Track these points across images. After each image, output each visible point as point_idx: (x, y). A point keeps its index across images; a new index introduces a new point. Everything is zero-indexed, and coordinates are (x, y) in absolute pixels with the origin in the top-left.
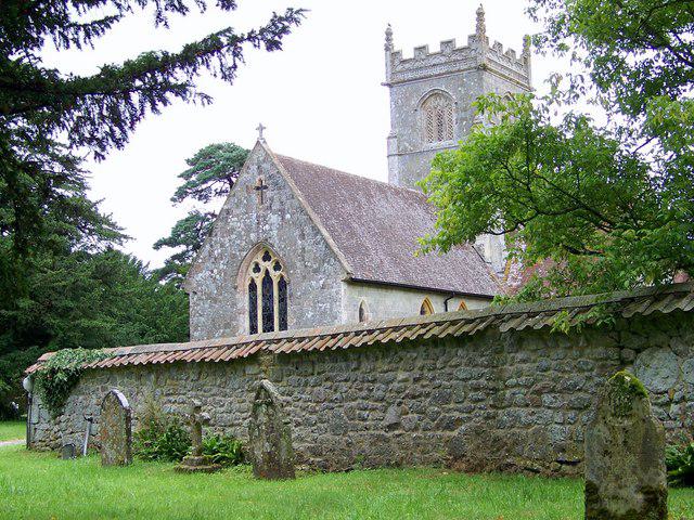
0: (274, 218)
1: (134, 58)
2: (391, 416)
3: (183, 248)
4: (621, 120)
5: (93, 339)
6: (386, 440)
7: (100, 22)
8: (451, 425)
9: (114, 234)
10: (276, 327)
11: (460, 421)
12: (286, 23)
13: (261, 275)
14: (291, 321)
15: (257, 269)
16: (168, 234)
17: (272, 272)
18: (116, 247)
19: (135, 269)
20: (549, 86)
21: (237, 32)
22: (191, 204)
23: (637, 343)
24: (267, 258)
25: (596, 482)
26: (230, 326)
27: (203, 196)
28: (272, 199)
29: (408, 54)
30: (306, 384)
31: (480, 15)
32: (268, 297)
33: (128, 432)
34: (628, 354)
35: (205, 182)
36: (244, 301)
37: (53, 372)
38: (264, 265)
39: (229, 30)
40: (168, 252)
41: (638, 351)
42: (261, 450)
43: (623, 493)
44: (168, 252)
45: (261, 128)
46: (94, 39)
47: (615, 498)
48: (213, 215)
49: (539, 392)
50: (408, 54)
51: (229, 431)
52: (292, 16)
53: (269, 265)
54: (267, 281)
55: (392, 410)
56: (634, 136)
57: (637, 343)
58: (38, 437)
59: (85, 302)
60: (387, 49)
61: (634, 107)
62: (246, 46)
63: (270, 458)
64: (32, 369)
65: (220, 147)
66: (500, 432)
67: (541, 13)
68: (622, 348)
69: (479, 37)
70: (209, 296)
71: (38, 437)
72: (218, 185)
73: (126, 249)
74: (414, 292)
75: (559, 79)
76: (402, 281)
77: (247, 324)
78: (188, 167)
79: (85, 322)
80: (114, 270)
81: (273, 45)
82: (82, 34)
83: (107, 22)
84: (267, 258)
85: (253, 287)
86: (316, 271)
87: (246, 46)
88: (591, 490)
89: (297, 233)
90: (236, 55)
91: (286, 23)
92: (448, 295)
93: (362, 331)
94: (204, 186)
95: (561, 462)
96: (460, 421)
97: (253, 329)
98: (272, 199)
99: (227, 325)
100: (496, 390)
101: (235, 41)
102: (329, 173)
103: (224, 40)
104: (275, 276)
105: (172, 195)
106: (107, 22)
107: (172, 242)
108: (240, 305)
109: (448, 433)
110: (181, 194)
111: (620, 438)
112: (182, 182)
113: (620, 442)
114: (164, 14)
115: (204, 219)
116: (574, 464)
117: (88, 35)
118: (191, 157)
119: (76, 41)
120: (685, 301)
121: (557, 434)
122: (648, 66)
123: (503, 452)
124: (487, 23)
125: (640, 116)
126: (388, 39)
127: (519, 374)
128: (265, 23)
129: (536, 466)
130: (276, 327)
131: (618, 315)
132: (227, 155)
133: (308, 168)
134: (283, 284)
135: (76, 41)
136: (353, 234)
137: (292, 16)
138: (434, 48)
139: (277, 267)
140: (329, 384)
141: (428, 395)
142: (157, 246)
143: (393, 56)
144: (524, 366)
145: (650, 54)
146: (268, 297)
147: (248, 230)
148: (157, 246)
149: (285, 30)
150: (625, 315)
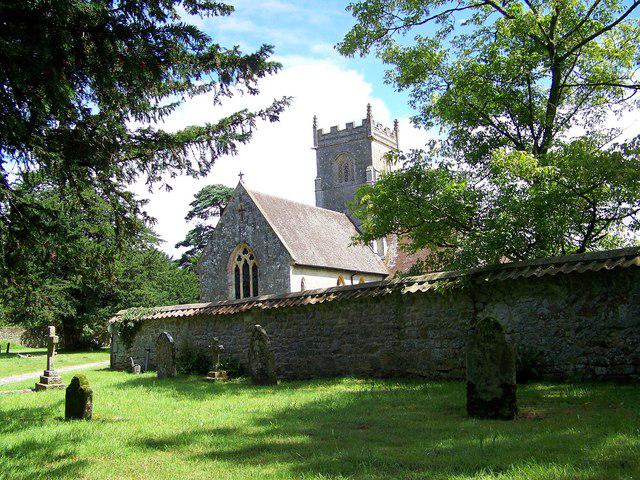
0: (249, 228)
1: (182, 129)
2: (335, 344)
3: (193, 247)
4: (465, 167)
5: (139, 301)
6: (332, 360)
7: (168, 107)
8: (371, 350)
9: (158, 241)
10: (251, 294)
11: (377, 348)
12: (282, 105)
13: (242, 262)
14: (260, 290)
15: (239, 259)
16: (183, 239)
17: (248, 259)
18: (156, 247)
19: (166, 259)
20: (428, 147)
21: (252, 110)
22: (196, 221)
23: (484, 299)
24: (245, 252)
25: (473, 382)
26: (224, 293)
27: (204, 216)
28: (248, 217)
29: (327, 130)
30: (282, 327)
31: (369, 107)
32: (246, 276)
33: (174, 357)
34: (479, 305)
35: (205, 207)
36: (232, 278)
37: (126, 321)
38: (244, 257)
39: (246, 110)
40: (184, 250)
41: (485, 304)
42: (255, 367)
43: (490, 388)
44: (184, 250)
45: (241, 175)
46: (165, 117)
47: (485, 391)
48: (210, 227)
49: (426, 329)
50: (327, 130)
51: (234, 356)
52: (286, 101)
53: (247, 257)
54: (246, 265)
55: (335, 343)
56: (474, 176)
57: (484, 299)
58: (117, 361)
59: (137, 278)
60: (314, 127)
61: (473, 159)
62: (258, 119)
63: (262, 372)
64: (113, 320)
65: (213, 187)
66: (403, 354)
67: (418, 104)
68: (475, 302)
69: (367, 121)
70: (211, 276)
71: (117, 361)
72: (213, 209)
73: (161, 248)
74: (325, 273)
75: (435, 143)
76: (327, 265)
77: (234, 292)
78: (195, 199)
79: (138, 292)
80: (154, 261)
81: (274, 119)
82: (157, 114)
83: (172, 106)
84: (245, 252)
85: (237, 270)
86: (274, 260)
87: (258, 119)
88: (471, 388)
89: (264, 237)
90: (251, 124)
91: (282, 105)
92: (353, 273)
93: (593, 261)
94: (205, 210)
95: (440, 371)
96: (377, 348)
97: (238, 295)
98: (248, 217)
99: (222, 293)
100: (399, 328)
101: (251, 116)
102: (282, 201)
103: (245, 117)
104: (251, 263)
105: (186, 215)
106: (172, 106)
107: (186, 244)
108: (229, 281)
109: (370, 355)
110: (191, 215)
111: (488, 355)
112: (192, 208)
113: (488, 358)
114: (220, 97)
115: (205, 229)
116: (447, 372)
117: (161, 114)
118: (197, 193)
119: (154, 118)
120: (513, 273)
121: (437, 354)
122: (481, 136)
123: (404, 366)
124: (373, 113)
125: (478, 164)
126: (369, 110)
127: (413, 319)
128: (269, 104)
129: (425, 374)
130: (251, 294)
131: (474, 283)
132: (218, 191)
133: (269, 198)
134: (255, 268)
135: (154, 118)
136: (296, 238)
137: (286, 101)
138: (342, 127)
139: (251, 258)
140: (296, 327)
141: (357, 333)
142: (177, 246)
143: (318, 135)
144: (417, 314)
145: (481, 129)
146: (246, 276)
147: (234, 235)
148: (177, 246)
149: (281, 109)
150: (478, 282)
